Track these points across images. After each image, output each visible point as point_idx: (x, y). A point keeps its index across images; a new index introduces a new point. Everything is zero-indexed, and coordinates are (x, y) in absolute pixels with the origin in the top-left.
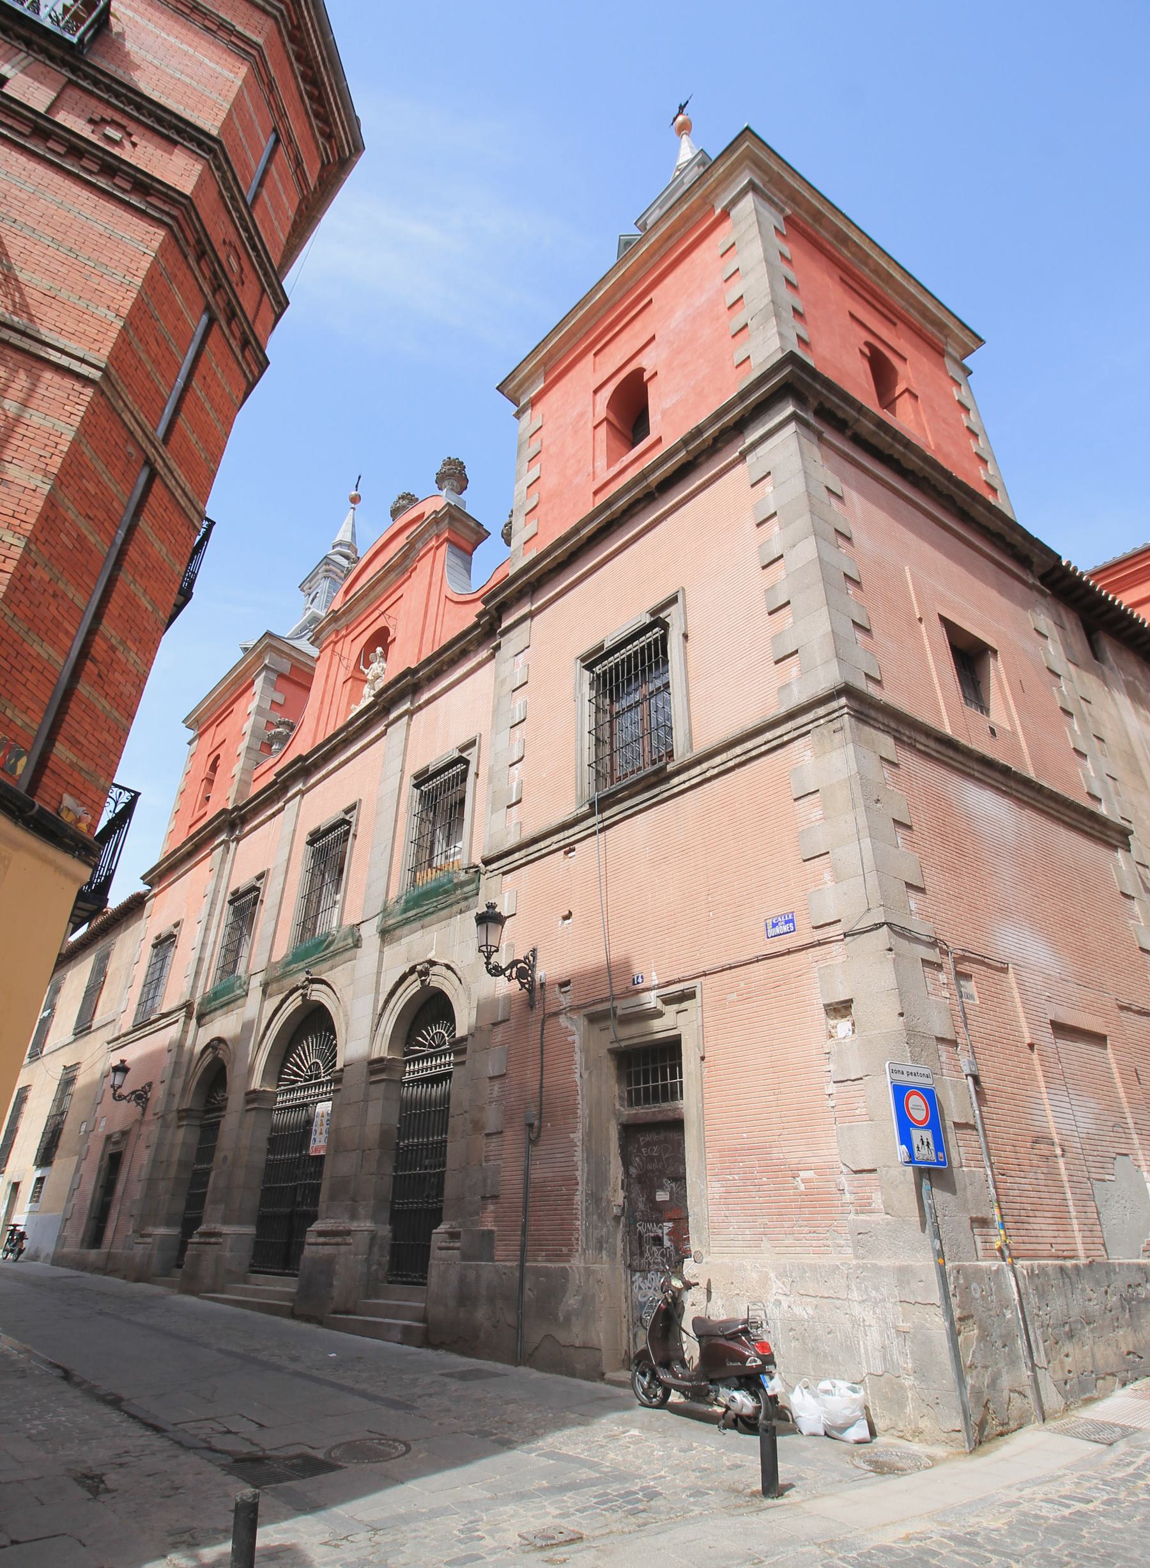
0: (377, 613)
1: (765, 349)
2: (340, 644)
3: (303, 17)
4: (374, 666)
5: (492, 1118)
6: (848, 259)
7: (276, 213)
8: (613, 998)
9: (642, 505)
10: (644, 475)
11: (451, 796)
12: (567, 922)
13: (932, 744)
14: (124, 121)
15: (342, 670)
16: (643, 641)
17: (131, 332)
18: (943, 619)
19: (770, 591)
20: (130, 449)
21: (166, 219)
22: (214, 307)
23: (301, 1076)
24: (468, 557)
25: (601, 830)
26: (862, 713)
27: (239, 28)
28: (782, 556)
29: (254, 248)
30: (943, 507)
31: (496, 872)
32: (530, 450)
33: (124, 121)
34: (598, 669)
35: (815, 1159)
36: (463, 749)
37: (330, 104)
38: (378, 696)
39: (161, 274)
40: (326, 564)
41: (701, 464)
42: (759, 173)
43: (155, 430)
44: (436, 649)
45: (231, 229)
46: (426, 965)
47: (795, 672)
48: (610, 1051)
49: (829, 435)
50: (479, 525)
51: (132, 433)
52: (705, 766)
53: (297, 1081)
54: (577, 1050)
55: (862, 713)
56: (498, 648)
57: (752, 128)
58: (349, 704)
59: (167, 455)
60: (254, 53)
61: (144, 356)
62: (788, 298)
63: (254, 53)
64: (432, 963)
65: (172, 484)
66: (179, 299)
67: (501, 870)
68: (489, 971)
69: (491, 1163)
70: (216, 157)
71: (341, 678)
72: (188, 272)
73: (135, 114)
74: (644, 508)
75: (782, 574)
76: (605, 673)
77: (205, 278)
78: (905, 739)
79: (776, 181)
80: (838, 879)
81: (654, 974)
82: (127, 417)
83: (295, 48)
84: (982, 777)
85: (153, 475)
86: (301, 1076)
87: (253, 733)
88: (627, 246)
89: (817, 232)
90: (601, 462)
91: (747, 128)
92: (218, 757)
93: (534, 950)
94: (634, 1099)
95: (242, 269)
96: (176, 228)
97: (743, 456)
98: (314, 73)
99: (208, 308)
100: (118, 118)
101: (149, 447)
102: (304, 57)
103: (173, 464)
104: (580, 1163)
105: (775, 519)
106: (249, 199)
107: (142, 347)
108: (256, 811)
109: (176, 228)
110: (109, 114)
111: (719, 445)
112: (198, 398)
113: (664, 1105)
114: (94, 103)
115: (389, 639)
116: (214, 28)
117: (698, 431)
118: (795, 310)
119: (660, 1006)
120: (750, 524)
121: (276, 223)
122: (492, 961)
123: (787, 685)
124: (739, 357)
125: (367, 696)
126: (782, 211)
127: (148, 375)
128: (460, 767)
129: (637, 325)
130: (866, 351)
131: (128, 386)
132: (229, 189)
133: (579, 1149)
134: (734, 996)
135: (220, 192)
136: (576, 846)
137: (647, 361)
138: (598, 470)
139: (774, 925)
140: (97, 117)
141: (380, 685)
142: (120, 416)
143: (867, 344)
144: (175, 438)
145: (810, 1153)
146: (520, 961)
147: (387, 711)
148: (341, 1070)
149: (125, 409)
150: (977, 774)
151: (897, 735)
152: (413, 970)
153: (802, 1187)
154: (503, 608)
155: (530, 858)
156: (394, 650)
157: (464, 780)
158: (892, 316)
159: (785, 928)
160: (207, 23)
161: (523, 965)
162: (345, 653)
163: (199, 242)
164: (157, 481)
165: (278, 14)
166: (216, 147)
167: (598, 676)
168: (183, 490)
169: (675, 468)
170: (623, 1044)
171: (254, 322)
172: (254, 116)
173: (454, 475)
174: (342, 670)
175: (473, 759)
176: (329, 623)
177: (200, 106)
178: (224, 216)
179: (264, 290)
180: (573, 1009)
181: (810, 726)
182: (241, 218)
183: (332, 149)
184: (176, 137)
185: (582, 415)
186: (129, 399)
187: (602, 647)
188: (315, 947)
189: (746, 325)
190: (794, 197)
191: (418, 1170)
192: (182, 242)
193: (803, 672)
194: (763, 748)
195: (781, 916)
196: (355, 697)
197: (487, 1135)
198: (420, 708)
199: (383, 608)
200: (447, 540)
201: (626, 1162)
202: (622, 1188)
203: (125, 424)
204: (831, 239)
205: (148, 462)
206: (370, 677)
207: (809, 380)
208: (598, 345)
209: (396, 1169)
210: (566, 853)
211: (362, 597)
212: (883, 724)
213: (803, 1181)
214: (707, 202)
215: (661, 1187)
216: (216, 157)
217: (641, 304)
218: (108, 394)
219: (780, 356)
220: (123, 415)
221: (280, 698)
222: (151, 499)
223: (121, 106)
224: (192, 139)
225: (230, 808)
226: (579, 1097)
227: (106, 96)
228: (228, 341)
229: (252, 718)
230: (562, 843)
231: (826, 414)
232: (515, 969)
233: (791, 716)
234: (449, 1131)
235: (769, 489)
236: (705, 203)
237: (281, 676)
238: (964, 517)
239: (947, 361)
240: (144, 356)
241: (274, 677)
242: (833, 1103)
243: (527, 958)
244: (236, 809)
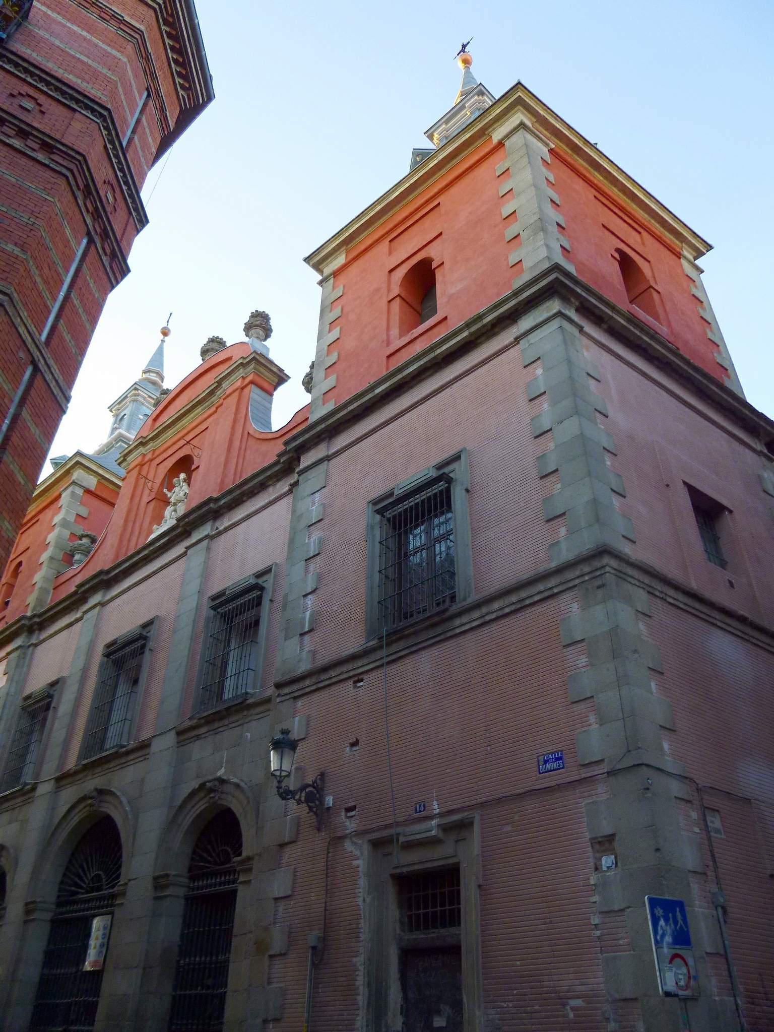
0: (182, 442)
1: (534, 256)
2: (146, 467)
3: (176, 9)
4: (176, 489)
5: (278, 943)
6: (599, 180)
7: (144, 152)
8: (398, 824)
9: (430, 372)
10: (432, 349)
11: (248, 616)
12: (355, 748)
13: (680, 597)
14: (36, 95)
15: (147, 492)
16: (430, 492)
17: (31, 263)
18: (685, 483)
19: (541, 458)
20: (22, 354)
21: (64, 171)
22: (93, 233)
23: (81, 888)
24: (269, 397)
25: (389, 663)
26: (620, 572)
27: (127, 18)
28: (551, 429)
29: (126, 183)
30: (684, 386)
31: (288, 697)
32: (331, 314)
33: (36, 95)
34: (388, 514)
35: (582, 988)
36: (259, 575)
37: (191, 67)
38: (179, 520)
39: (57, 215)
40: (136, 389)
41: (481, 343)
42: (529, 116)
43: (40, 335)
44: (238, 482)
45: (110, 172)
46: (217, 783)
47: (563, 531)
48: (393, 876)
49: (589, 328)
50: (281, 370)
51: (24, 341)
52: (484, 610)
53: (78, 893)
54: (361, 874)
55: (620, 572)
56: (296, 484)
57: (523, 82)
58: (151, 524)
59: (48, 355)
60: (137, 36)
61: (38, 280)
62: (554, 216)
63: (137, 36)
64: (222, 781)
65: (49, 377)
66: (68, 231)
67: (292, 695)
68: (280, 795)
69: (274, 985)
70: (105, 120)
71: (146, 499)
72: (77, 209)
73: (45, 89)
74: (431, 375)
75: (552, 445)
76: (394, 517)
77: (88, 211)
78: (657, 593)
79: (543, 122)
80: (602, 722)
81: (435, 803)
82: (22, 330)
83: (168, 29)
84: (724, 626)
85: (36, 369)
86: (81, 888)
87: (58, 546)
88: (421, 157)
89: (576, 160)
90: (395, 332)
91: (519, 83)
92: (20, 564)
93: (322, 775)
94: (413, 923)
95: (115, 200)
96: (71, 178)
97: (517, 340)
98: (181, 47)
99: (88, 233)
100: (32, 92)
101: (36, 350)
102: (176, 37)
103: (51, 362)
104: (361, 988)
105: (544, 397)
106: (124, 144)
107: (37, 272)
108: (53, 619)
109: (71, 178)
110: (25, 89)
111: (496, 330)
112: (74, 306)
113: (442, 931)
114: (14, 80)
115: (193, 467)
116: (108, 18)
117: (480, 317)
118: (558, 224)
119: (441, 835)
120: (522, 400)
121: (142, 159)
122: (283, 785)
123: (557, 543)
124: (513, 260)
125: (170, 519)
126: (547, 145)
127: (40, 294)
128: (255, 594)
129: (427, 222)
130: (617, 256)
131: (25, 305)
132: (112, 142)
133: (361, 973)
134: (508, 828)
135: (105, 147)
136: (365, 677)
137: (434, 252)
138: (392, 337)
139: (546, 762)
140: (15, 93)
141: (182, 510)
142: (17, 329)
143: (618, 250)
144: (55, 341)
145: (577, 982)
146: (309, 786)
147: (186, 534)
148: (126, 884)
149: (21, 324)
150: (719, 624)
151: (651, 590)
152: (202, 786)
153: (571, 1015)
154: (303, 448)
155: (320, 685)
156: (197, 476)
157: (259, 604)
158: (638, 226)
159: (555, 765)
160: (103, 15)
161: (311, 789)
162: (150, 477)
163: (87, 186)
164: (39, 376)
165: (157, 7)
166: (106, 113)
167: (389, 520)
168: (57, 381)
169: (459, 345)
170: (405, 870)
171: (121, 239)
172: (133, 82)
173: (259, 324)
174: (147, 492)
175: (268, 586)
176: (136, 447)
177: (94, 80)
178: (106, 163)
179: (130, 213)
180: (359, 834)
181: (577, 582)
182: (119, 162)
183: (189, 99)
184: (75, 106)
185: (377, 290)
186: (24, 315)
187: (392, 494)
188: (100, 755)
189: (519, 235)
190: (557, 134)
191: (199, 991)
192: (75, 188)
193: (571, 532)
194: (536, 598)
195: (551, 753)
196: (158, 518)
197: (272, 957)
198: (220, 534)
199: (188, 438)
200: (252, 382)
201: (404, 987)
202: (401, 1013)
203: (20, 335)
204: (587, 166)
205: (34, 363)
206: (172, 500)
207: (572, 285)
208: (394, 235)
209: (175, 989)
210: (355, 682)
211: (169, 426)
212: (639, 581)
213: (573, 1009)
214: (483, 132)
215: (439, 1012)
216: (105, 120)
217: (431, 207)
218: (10, 313)
219: (546, 265)
220: (20, 329)
221: (84, 512)
222: (33, 392)
223: (35, 83)
224: (87, 107)
225: (29, 614)
226: (362, 921)
227: (23, 76)
228: (100, 256)
229: (57, 530)
230: (351, 674)
231: (586, 310)
232: (304, 794)
233: (559, 570)
234: (232, 951)
235: (539, 371)
236: (485, 134)
237: (88, 491)
238: (702, 393)
239: (683, 261)
240: (38, 280)
241: (80, 492)
242: (598, 933)
243: (315, 782)
244: (34, 616)
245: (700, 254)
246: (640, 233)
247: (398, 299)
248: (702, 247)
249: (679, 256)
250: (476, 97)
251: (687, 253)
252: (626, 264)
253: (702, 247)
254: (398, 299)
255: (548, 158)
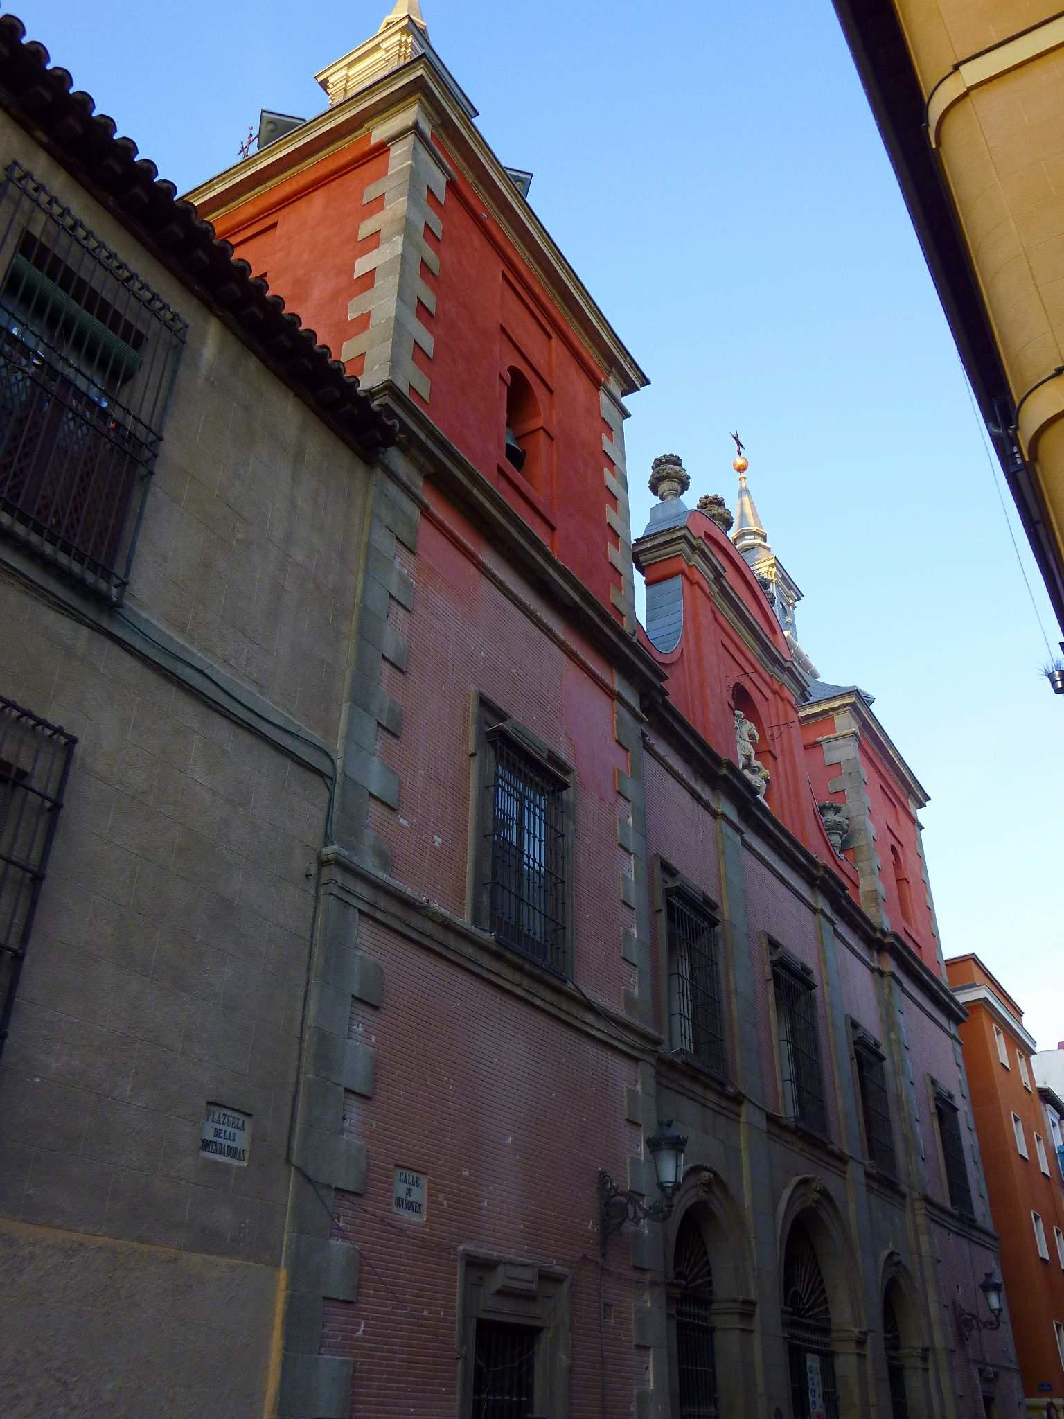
130: (508, 377)
158: (551, 327)
245: (630, 388)
246: (550, 337)
247: (411, 138)
248: (633, 380)
249: (597, 384)
250: (398, 37)
251: (614, 386)
252: (519, 393)
253: (633, 380)
254: (411, 138)
255: (441, 193)
